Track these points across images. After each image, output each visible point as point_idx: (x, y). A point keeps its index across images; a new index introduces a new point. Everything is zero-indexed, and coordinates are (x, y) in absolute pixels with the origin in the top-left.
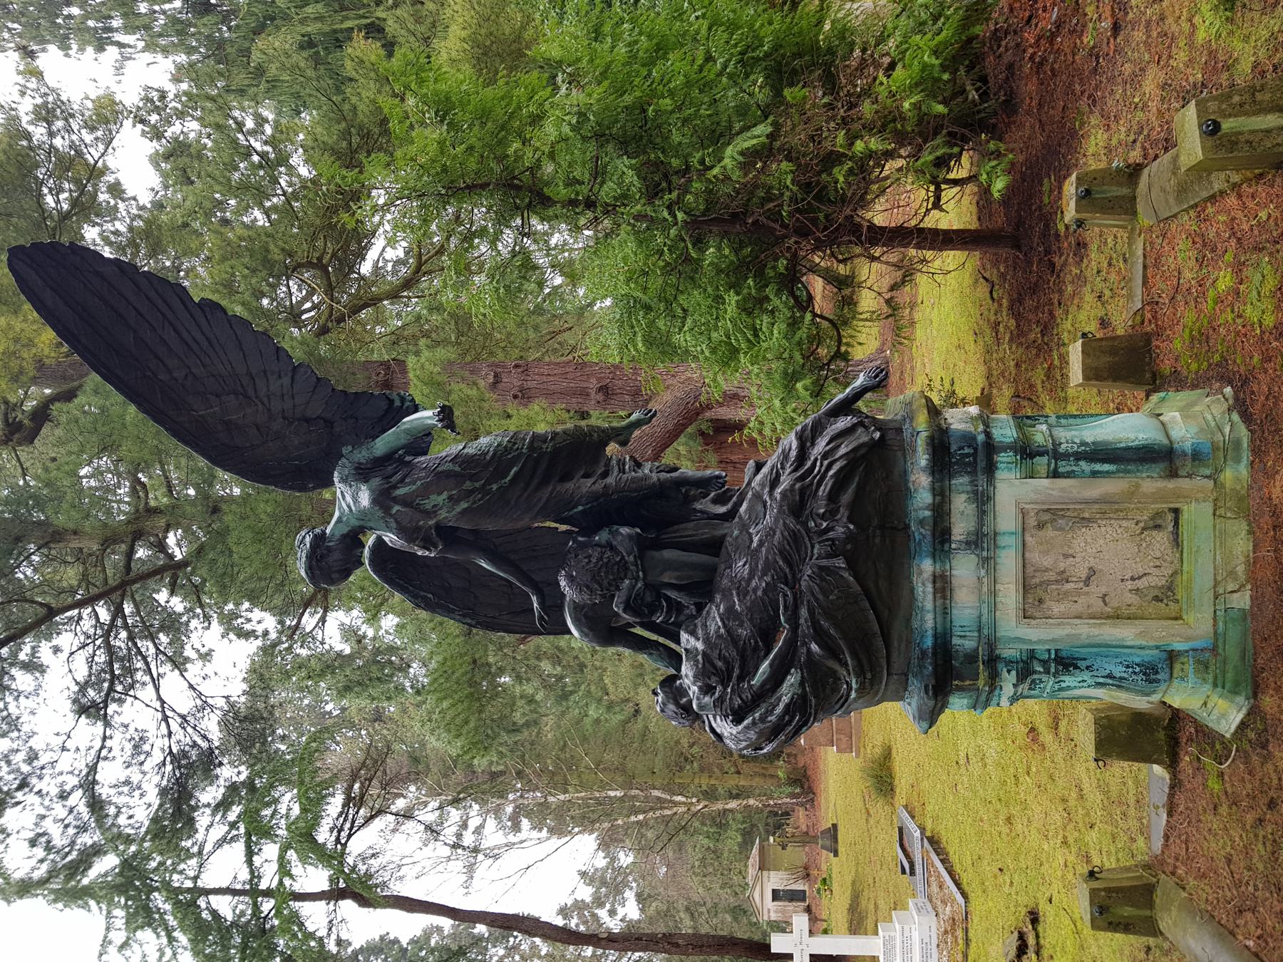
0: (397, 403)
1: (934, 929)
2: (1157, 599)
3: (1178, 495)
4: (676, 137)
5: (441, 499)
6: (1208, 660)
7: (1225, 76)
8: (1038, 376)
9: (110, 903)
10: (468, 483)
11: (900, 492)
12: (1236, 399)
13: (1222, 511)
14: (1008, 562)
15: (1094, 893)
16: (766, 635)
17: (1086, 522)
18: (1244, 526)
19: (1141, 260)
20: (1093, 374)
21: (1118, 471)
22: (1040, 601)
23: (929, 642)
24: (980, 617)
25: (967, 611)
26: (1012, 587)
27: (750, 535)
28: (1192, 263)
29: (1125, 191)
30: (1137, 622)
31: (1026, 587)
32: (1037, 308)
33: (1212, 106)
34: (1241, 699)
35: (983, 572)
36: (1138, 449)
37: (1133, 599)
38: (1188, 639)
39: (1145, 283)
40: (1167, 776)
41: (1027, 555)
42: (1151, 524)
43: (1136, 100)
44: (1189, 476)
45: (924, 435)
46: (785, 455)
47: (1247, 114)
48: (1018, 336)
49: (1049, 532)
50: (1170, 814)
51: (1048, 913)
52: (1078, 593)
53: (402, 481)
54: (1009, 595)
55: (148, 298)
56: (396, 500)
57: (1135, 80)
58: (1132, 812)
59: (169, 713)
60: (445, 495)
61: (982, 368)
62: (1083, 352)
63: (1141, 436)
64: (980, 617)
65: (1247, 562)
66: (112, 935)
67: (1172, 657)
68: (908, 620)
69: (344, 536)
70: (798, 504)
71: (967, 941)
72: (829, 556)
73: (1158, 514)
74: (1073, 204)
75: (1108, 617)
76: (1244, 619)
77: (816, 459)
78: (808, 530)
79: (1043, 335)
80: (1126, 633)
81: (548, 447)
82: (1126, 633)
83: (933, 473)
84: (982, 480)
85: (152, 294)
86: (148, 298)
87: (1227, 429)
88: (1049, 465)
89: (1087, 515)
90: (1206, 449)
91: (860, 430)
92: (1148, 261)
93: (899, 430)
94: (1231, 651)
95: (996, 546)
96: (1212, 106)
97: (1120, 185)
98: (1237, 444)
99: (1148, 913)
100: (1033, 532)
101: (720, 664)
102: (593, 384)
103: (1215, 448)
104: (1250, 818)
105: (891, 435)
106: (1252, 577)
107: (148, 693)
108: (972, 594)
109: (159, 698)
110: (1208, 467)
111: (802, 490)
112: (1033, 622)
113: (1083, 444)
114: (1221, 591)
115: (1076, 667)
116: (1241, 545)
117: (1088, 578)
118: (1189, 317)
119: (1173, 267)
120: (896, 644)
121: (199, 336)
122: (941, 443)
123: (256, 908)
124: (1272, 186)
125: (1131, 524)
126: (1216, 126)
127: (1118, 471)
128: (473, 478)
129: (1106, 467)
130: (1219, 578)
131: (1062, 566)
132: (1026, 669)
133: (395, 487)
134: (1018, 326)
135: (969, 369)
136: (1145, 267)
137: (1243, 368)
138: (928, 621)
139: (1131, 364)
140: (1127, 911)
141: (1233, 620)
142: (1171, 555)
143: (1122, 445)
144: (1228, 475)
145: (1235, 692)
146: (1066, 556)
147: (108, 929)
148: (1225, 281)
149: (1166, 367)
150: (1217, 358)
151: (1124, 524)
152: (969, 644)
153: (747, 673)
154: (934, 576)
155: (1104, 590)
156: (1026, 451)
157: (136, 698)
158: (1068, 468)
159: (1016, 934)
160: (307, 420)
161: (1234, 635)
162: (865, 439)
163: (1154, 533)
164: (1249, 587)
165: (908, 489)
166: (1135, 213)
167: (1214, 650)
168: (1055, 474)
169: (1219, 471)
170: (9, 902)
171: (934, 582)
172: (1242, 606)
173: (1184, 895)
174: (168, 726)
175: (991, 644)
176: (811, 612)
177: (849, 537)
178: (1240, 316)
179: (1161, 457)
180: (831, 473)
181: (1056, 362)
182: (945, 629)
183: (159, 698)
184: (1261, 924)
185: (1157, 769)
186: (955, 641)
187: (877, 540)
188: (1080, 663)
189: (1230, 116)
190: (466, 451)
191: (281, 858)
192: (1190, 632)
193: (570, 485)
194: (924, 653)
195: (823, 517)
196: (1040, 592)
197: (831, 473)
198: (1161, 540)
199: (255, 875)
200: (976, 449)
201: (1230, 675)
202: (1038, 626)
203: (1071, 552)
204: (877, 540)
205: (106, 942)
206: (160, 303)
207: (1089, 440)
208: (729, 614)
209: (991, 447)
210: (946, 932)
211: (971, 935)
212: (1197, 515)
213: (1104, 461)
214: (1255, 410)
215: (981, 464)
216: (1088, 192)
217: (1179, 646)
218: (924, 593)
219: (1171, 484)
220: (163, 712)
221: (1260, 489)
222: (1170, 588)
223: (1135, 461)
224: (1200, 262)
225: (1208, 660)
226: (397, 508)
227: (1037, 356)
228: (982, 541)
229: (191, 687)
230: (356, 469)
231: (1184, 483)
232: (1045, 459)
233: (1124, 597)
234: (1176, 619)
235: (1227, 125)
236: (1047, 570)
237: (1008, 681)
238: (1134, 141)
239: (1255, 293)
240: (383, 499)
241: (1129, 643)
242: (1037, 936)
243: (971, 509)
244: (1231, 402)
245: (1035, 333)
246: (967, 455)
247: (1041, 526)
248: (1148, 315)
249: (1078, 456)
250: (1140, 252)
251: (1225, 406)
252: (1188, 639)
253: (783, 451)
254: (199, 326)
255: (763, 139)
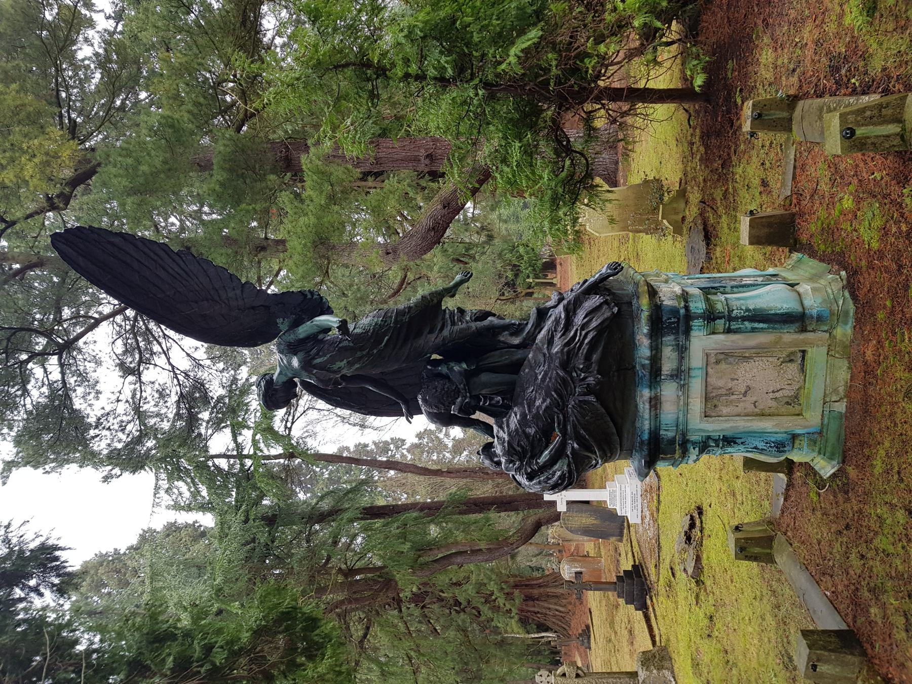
0: (309, 296)
1: (639, 486)
2: (788, 403)
3: (805, 342)
4: (476, 38)
5: (342, 364)
6: (816, 439)
7: (862, 63)
8: (718, 194)
9: (158, 469)
10: (359, 353)
11: (631, 346)
12: (849, 282)
13: (833, 353)
14: (696, 386)
15: (737, 540)
16: (546, 435)
17: (746, 359)
18: (846, 363)
19: (792, 162)
20: (755, 240)
21: (768, 328)
22: (715, 406)
23: (646, 437)
24: (678, 418)
25: (670, 416)
26: (699, 400)
27: (536, 374)
28: (827, 180)
29: (785, 114)
30: (774, 418)
31: (707, 398)
32: (719, 147)
33: (851, 118)
34: (834, 463)
35: (680, 393)
36: (782, 315)
37: (774, 404)
38: (805, 427)
39: (794, 178)
40: (786, 479)
41: (709, 379)
42: (787, 359)
43: (797, 40)
44: (814, 331)
45: (647, 313)
46: (557, 321)
47: (874, 124)
48: (706, 160)
49: (723, 366)
50: (785, 500)
51: (709, 513)
52: (739, 401)
53: (317, 354)
54: (697, 405)
55: (144, 253)
56: (315, 367)
57: (797, 24)
58: (762, 484)
59: (178, 372)
60: (345, 361)
61: (681, 166)
62: (750, 226)
63: (785, 306)
64: (678, 418)
65: (846, 386)
66: (160, 482)
67: (794, 437)
68: (634, 423)
69: (284, 383)
70: (567, 362)
71: (659, 502)
72: (585, 394)
73: (792, 353)
74: (749, 123)
75: (757, 415)
76: (841, 419)
77: (577, 330)
78: (572, 378)
79: (723, 168)
80: (767, 425)
81: (406, 318)
82: (767, 425)
83: (651, 338)
84: (682, 338)
85: (146, 250)
86: (144, 253)
87: (841, 303)
88: (725, 324)
89: (747, 355)
90: (826, 314)
91: (605, 307)
92: (797, 164)
93: (630, 304)
94: (832, 436)
95: (689, 376)
96: (851, 118)
97: (783, 110)
98: (846, 313)
99: (769, 551)
100: (713, 366)
101: (519, 449)
102: (423, 153)
103: (832, 313)
104: (834, 527)
105: (625, 308)
106: (847, 395)
107: (161, 360)
108: (674, 405)
109: (170, 364)
110: (826, 325)
111: (569, 352)
112: (710, 419)
113: (748, 310)
114: (828, 400)
115: (735, 443)
116: (843, 375)
117: (746, 392)
118: (822, 213)
119: (813, 175)
120: (626, 435)
121: (180, 271)
122: (657, 310)
123: (242, 465)
124: (886, 159)
125: (775, 360)
126: (853, 132)
127: (768, 328)
128: (361, 349)
129: (761, 325)
130: (827, 392)
131: (730, 385)
132: (704, 446)
133: (314, 358)
134: (706, 153)
135: (672, 161)
136: (795, 167)
137: (854, 263)
138: (645, 424)
139: (780, 233)
140: (757, 550)
141: (834, 418)
142: (798, 377)
143: (773, 312)
144: (839, 332)
145: (831, 458)
146: (733, 379)
147: (157, 480)
148: (848, 203)
149: (804, 238)
150: (838, 249)
151: (770, 359)
152: (670, 434)
153: (537, 454)
154: (651, 398)
155: (755, 399)
156: (710, 316)
157: (156, 365)
158: (737, 326)
159: (689, 517)
160: (253, 308)
161: (834, 426)
162: (608, 314)
163: (789, 364)
164: (845, 400)
165: (635, 344)
166: (790, 130)
167: (820, 433)
168: (729, 331)
169: (833, 328)
170: (97, 469)
171: (650, 402)
172: (840, 410)
173: (791, 549)
174: (178, 380)
175: (684, 435)
176: (574, 427)
177: (598, 383)
178: (856, 231)
179: (798, 320)
180: (586, 341)
181: (731, 190)
182: (656, 426)
183: (170, 364)
184: (834, 585)
185: (781, 475)
186: (662, 432)
187: (615, 378)
188: (737, 441)
189: (863, 125)
190: (355, 331)
191: (254, 440)
192: (807, 423)
193: (421, 341)
194: (642, 442)
195: (581, 370)
196: (715, 401)
197: (586, 341)
198: (793, 368)
199: (239, 447)
200: (679, 319)
201: (829, 449)
202: (713, 422)
203: (736, 377)
204: (615, 378)
205: (157, 488)
206: (152, 254)
207: (751, 308)
208: (523, 422)
209: (689, 317)
210: (646, 491)
211: (661, 498)
212: (817, 355)
213: (759, 322)
214: (861, 294)
215: (682, 328)
216: (760, 115)
217: (798, 431)
218: (644, 408)
219: (802, 336)
220: (174, 372)
221: (858, 345)
222: (796, 397)
223: (779, 322)
224: (833, 182)
225: (816, 439)
226: (315, 371)
227: (718, 180)
228: (680, 375)
229: (188, 355)
230: (288, 346)
231: (810, 336)
232: (723, 321)
233: (767, 403)
234: (798, 415)
235: (860, 132)
236: (720, 388)
237: (693, 453)
238: (794, 70)
239: (867, 223)
240: (307, 365)
241: (769, 431)
242: (701, 522)
243: (675, 355)
244: (845, 282)
245: (717, 164)
246: (674, 323)
247: (718, 362)
248: (795, 201)
249: (744, 319)
250: (792, 157)
251: (841, 285)
252: (805, 427)
253: (556, 318)
254: (178, 264)
255: (536, 40)
